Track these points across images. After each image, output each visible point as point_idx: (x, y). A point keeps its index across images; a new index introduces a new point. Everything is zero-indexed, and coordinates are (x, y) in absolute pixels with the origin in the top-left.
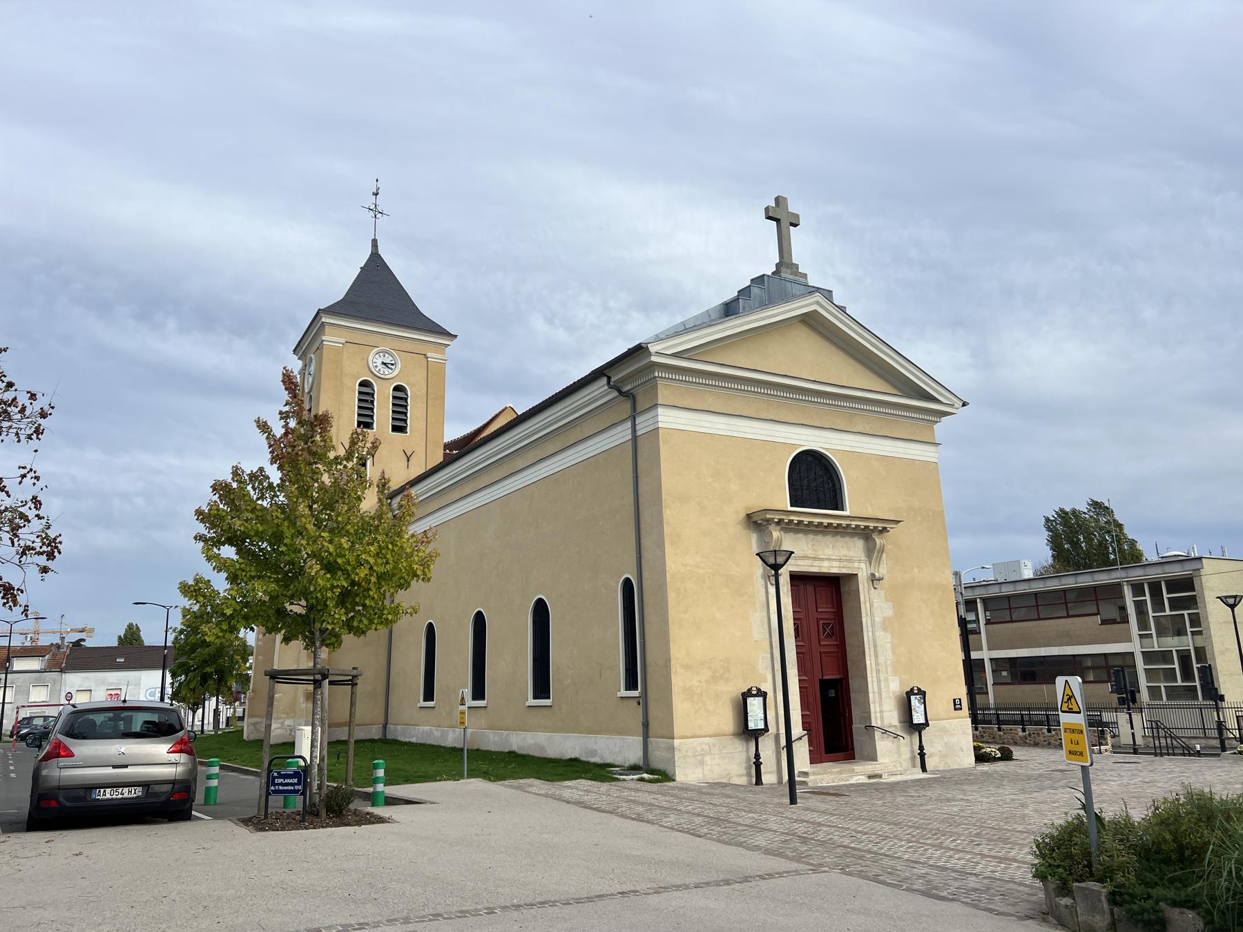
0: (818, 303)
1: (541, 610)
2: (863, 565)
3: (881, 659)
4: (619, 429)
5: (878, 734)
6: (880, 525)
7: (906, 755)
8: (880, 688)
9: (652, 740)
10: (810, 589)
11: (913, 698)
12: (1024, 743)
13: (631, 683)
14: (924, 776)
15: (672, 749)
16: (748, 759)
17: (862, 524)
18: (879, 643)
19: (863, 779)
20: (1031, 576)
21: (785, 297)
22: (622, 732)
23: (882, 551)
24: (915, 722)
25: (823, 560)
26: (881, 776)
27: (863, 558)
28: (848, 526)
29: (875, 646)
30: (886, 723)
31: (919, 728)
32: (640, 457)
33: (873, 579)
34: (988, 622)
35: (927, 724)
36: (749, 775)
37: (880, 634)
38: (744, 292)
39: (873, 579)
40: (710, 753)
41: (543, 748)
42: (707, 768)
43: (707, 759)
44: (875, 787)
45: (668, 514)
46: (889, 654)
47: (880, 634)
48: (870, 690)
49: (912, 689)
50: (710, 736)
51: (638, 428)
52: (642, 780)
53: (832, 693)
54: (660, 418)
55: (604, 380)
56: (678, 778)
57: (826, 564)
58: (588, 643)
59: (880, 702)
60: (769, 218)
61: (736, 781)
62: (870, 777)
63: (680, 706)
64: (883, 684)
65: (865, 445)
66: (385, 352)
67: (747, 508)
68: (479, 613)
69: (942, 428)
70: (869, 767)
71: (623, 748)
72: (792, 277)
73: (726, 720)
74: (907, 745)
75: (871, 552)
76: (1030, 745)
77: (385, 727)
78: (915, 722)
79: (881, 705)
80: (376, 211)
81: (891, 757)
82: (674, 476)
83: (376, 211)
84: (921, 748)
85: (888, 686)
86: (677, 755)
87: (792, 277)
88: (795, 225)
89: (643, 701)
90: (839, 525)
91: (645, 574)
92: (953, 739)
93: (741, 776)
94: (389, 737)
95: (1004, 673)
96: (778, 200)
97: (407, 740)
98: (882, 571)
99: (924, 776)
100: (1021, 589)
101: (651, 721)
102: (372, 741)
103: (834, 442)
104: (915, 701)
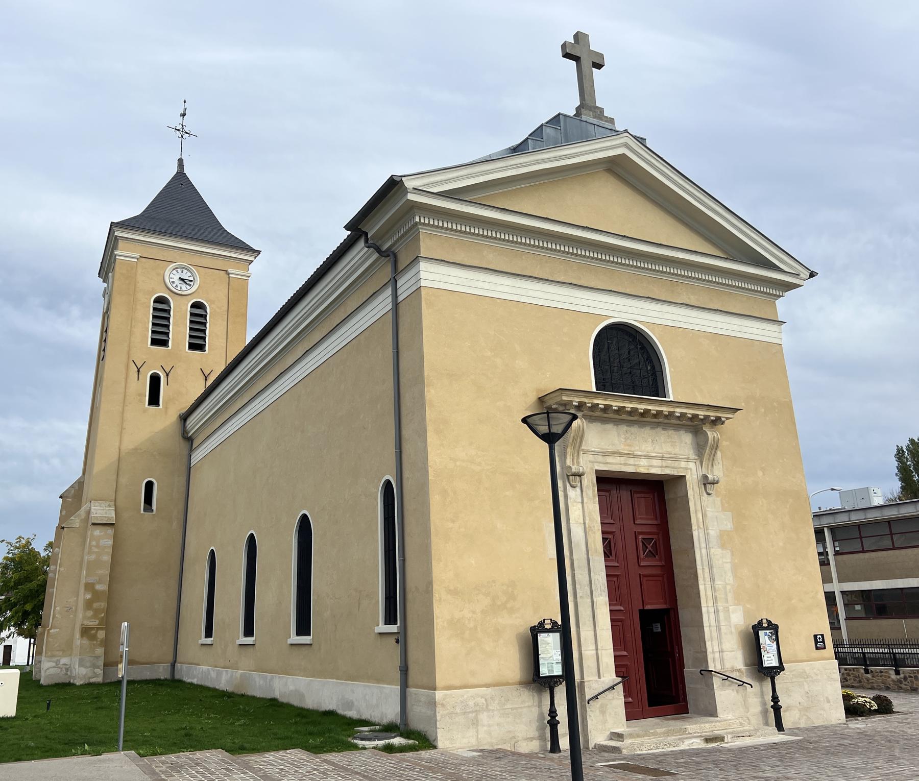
0: (626, 145)
1: (304, 526)
2: (692, 465)
3: (719, 583)
4: (380, 298)
5: (717, 681)
6: (713, 414)
7: (755, 708)
8: (718, 620)
9: (411, 690)
10: (625, 494)
11: (761, 633)
12: (898, 688)
13: (390, 618)
14: (780, 738)
15: (433, 704)
16: (541, 716)
17: (690, 412)
18: (716, 563)
19: (698, 744)
20: (881, 503)
21: (585, 138)
22: (379, 680)
23: (716, 446)
24: (766, 664)
25: (640, 457)
26: (722, 739)
27: (692, 456)
28: (671, 414)
29: (711, 567)
30: (728, 665)
31: (771, 673)
32: (401, 325)
33: (706, 483)
34: (837, 553)
35: (781, 668)
36: (542, 738)
37: (716, 551)
38: (538, 133)
39: (706, 483)
40: (487, 710)
41: (302, 696)
42: (482, 730)
43: (484, 717)
44: (714, 755)
45: (431, 394)
46: (730, 578)
47: (716, 551)
48: (706, 623)
49: (760, 622)
50: (487, 686)
51: (399, 292)
52: (389, 749)
53: (657, 628)
54: (423, 275)
55: (361, 243)
56: (440, 744)
57: (644, 462)
58: (349, 566)
59: (720, 643)
60: (567, 55)
61: (525, 747)
62: (707, 740)
63: (446, 646)
64: (721, 615)
65: (691, 320)
66: (183, 268)
67: (538, 390)
68: (252, 535)
69: (784, 305)
70: (706, 726)
71: (377, 701)
72: (595, 121)
73: (511, 664)
74: (756, 696)
75: (703, 450)
76: (906, 691)
77: (173, 666)
78: (766, 664)
79: (720, 642)
80: (182, 132)
81: (735, 713)
82: (438, 347)
83: (182, 132)
84: (775, 699)
85: (728, 618)
86: (440, 712)
87: (595, 121)
88: (599, 66)
89: (402, 639)
90: (659, 413)
91: (406, 474)
92: (816, 688)
93: (531, 739)
94: (177, 677)
95: (858, 607)
96: (577, 36)
97: (189, 681)
98: (717, 472)
99: (780, 738)
100: (872, 516)
101: (410, 669)
102: (157, 683)
103: (652, 314)
104: (764, 637)
